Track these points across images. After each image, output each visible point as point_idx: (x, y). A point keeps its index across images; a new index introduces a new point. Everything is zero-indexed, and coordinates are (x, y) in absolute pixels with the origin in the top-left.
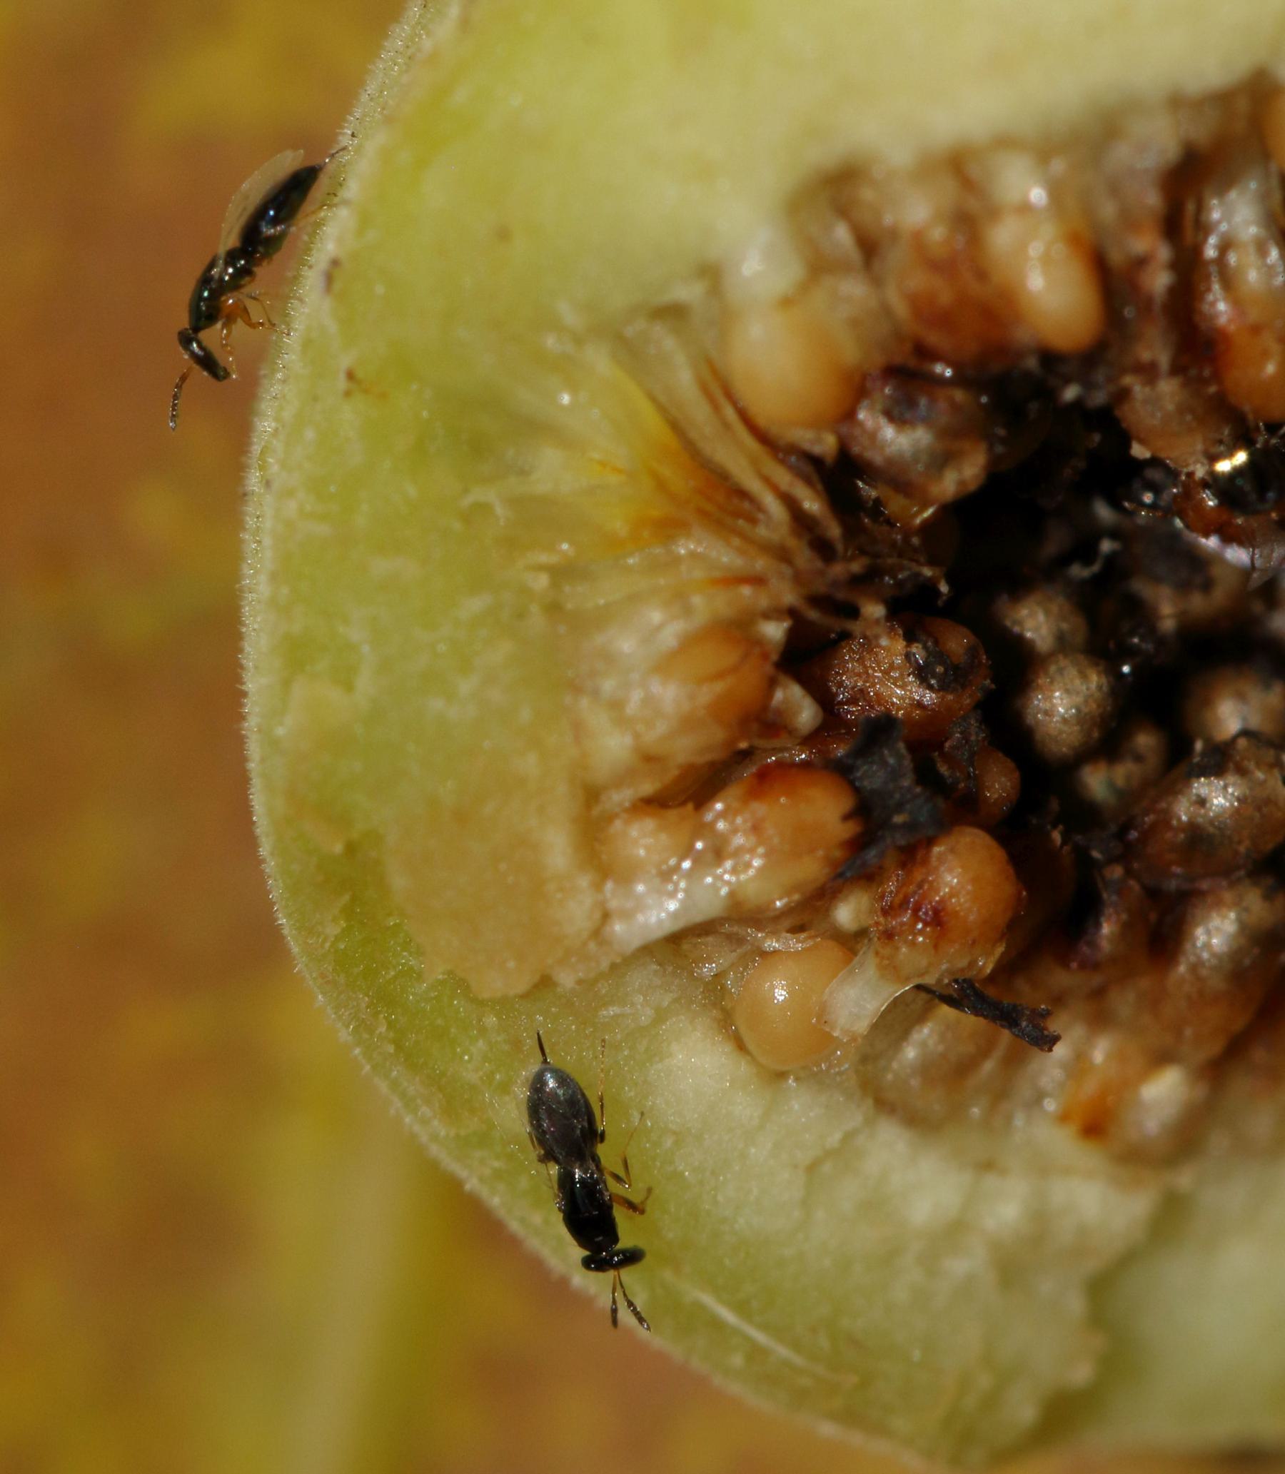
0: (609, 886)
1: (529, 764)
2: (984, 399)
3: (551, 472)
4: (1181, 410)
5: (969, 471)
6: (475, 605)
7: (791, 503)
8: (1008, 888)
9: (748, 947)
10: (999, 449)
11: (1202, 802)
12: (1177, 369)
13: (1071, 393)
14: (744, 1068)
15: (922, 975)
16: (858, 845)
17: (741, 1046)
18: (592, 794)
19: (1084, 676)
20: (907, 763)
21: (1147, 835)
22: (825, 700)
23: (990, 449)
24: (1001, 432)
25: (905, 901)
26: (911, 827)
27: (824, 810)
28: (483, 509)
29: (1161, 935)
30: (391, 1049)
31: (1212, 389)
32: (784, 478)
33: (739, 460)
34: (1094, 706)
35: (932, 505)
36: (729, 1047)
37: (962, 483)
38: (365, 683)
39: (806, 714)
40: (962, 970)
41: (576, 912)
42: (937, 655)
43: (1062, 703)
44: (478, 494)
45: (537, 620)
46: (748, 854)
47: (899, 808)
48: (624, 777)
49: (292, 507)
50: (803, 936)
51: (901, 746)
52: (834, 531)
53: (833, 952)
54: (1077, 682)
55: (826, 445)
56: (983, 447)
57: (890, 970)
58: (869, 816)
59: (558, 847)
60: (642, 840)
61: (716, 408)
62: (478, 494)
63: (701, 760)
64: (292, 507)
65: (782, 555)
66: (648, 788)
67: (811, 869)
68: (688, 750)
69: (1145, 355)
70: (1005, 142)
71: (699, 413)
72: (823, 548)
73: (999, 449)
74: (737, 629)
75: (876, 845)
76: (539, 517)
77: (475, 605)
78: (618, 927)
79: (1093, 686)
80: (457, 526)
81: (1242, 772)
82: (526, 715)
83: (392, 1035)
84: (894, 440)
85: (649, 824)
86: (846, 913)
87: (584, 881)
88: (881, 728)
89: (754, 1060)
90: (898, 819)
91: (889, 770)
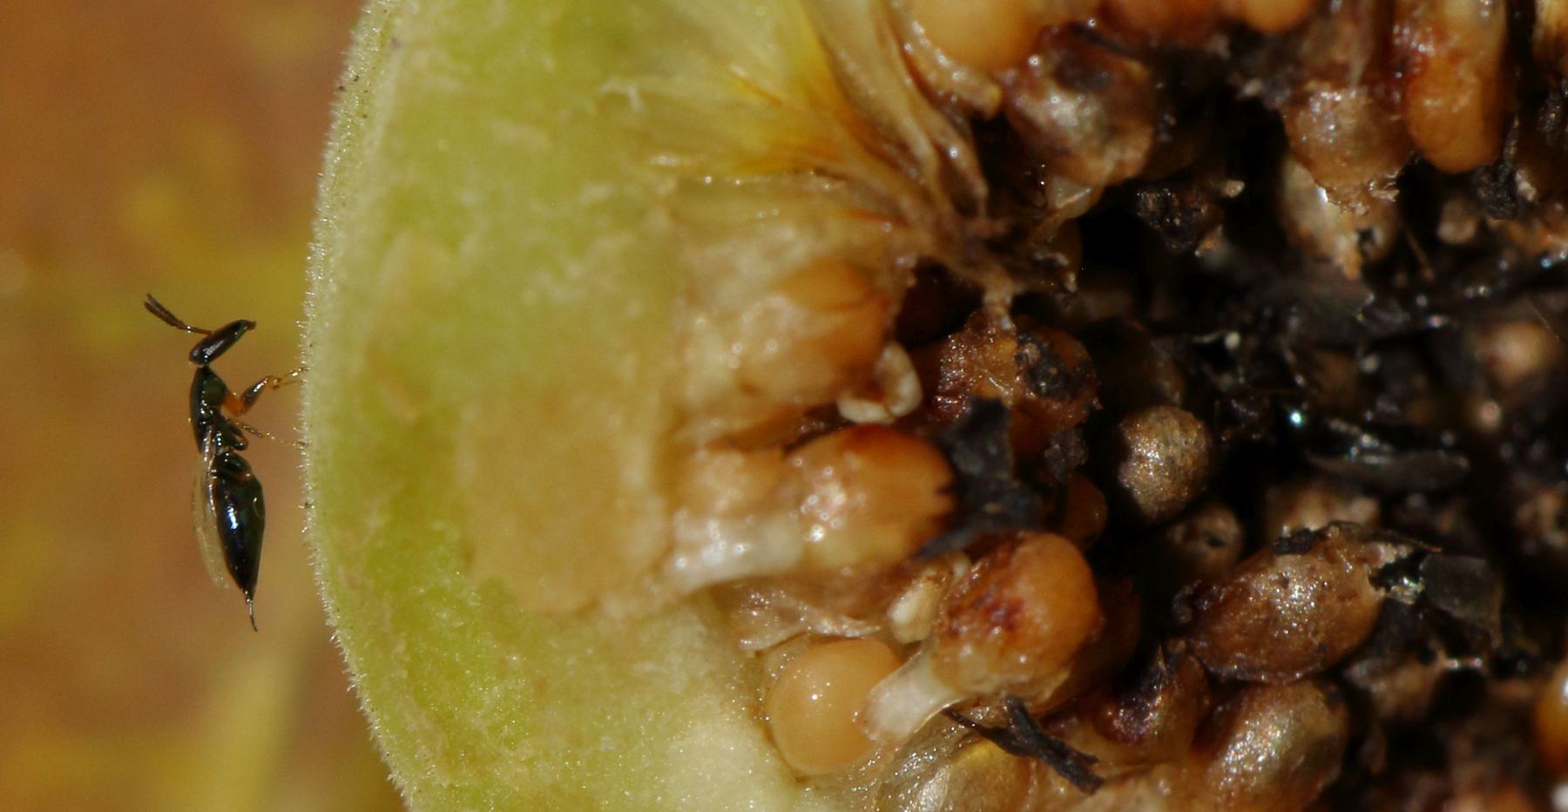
1: (627, 367)
2: (1160, 86)
3: (691, 83)
4: (1361, 135)
5: (1127, 155)
6: (597, 192)
7: (942, 153)
8: (1088, 607)
9: (795, 629)
10: (1164, 137)
12: (1365, 81)
13: (1251, 88)
14: (769, 760)
15: (979, 682)
16: (949, 523)
17: (769, 737)
18: (680, 417)
19: (1184, 431)
20: (1009, 456)
21: (1218, 609)
23: (1156, 134)
24: (1172, 121)
25: (980, 600)
26: (1000, 518)
27: (920, 483)
28: (621, 100)
29: (1208, 733)
30: (404, 674)
31: (1395, 118)
32: (936, 120)
34: (1190, 462)
35: (1085, 185)
37: (1120, 164)
38: (470, 246)
39: (907, 389)
40: (1022, 685)
41: (641, 540)
42: (1049, 356)
43: (1157, 455)
44: (613, 85)
45: (660, 221)
47: (995, 497)
48: (714, 407)
50: (860, 623)
51: (1006, 437)
52: (980, 189)
53: (883, 652)
54: (1177, 433)
55: (989, 97)
56: (1149, 131)
58: (963, 498)
59: (636, 466)
60: (725, 480)
61: (882, 40)
62: (613, 85)
63: (798, 400)
65: (925, 197)
66: (739, 424)
69: (1339, 56)
71: (865, 31)
72: (965, 207)
73: (1164, 137)
74: (859, 269)
75: (966, 527)
76: (666, 126)
77: (597, 192)
78: (682, 563)
80: (591, 109)
81: (1332, 560)
83: (407, 659)
84: (1062, 110)
85: (737, 459)
86: (910, 608)
87: (655, 504)
88: (988, 412)
90: (991, 508)
91: (988, 463)
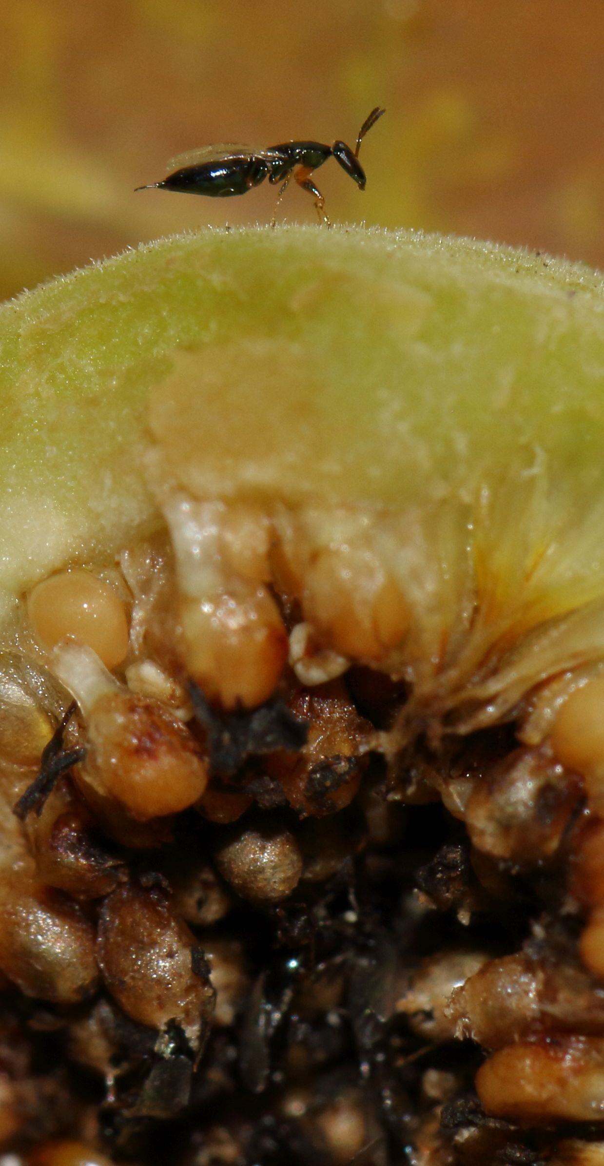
0: (221, 507)
1: (332, 466)
2: (540, 862)
4: (504, 1012)
5: (488, 838)
6: (461, 444)
8: (153, 809)
9: (136, 591)
10: (502, 866)
11: (170, 955)
12: (544, 1014)
13: (538, 931)
14: (38, 572)
16: (215, 705)
17: (56, 572)
20: (264, 751)
21: (151, 906)
22: (322, 691)
23: (505, 860)
24: (515, 870)
27: (245, 684)
28: (530, 461)
29: (58, 898)
30: (102, 301)
31: (516, 1037)
32: (515, 696)
33: (532, 664)
34: (260, 885)
36: (58, 565)
38: (421, 350)
39: (315, 675)
40: (95, 760)
41: (202, 477)
43: (265, 860)
44: (541, 456)
45: (440, 491)
46: (223, 621)
47: (234, 740)
48: (302, 531)
49: (560, 313)
50: (141, 640)
51: (279, 748)
52: (463, 729)
53: (119, 656)
57: (104, 704)
58: (236, 715)
59: (257, 473)
60: (247, 539)
62: (541, 456)
64: (560, 313)
65: (458, 688)
66: (288, 550)
67: (201, 663)
68: (319, 589)
69: (562, 996)
70: (314, 621)
72: (450, 717)
73: (502, 866)
74: (403, 638)
75: (212, 718)
77: (461, 444)
78: (186, 507)
79: (276, 886)
80: (523, 440)
81: (188, 990)
82: (375, 472)
85: (262, 548)
86: (152, 676)
87: (229, 487)
88: (297, 735)
89: (42, 580)
90: (226, 737)
